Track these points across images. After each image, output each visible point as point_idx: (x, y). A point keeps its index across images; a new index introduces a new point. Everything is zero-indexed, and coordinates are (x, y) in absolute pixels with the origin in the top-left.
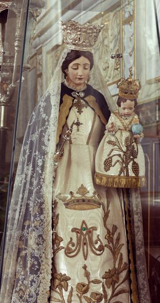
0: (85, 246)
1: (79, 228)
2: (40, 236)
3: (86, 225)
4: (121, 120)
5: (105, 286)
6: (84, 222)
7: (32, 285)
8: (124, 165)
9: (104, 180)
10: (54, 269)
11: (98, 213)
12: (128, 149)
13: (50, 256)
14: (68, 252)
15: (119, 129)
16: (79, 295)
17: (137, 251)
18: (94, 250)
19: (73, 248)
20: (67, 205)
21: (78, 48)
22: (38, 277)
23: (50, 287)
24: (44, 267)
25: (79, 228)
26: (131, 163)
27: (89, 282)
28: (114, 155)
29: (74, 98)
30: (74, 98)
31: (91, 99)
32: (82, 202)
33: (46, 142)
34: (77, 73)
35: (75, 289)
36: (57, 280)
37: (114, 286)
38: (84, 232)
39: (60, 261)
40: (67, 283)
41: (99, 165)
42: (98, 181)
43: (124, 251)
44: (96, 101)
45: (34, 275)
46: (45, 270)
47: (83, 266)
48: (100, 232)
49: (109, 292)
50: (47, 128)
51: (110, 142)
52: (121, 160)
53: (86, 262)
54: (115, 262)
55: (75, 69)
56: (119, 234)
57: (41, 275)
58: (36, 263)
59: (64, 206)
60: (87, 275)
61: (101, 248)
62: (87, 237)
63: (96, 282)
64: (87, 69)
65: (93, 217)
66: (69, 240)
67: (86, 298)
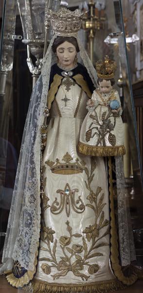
0: (68, 205)
1: (63, 190)
2: (32, 196)
3: (69, 187)
4: (101, 97)
5: (86, 240)
6: (67, 185)
7: (26, 236)
8: (101, 137)
9: (85, 150)
10: (43, 224)
11: (82, 177)
12: (104, 123)
13: (39, 213)
14: (53, 210)
15: (99, 104)
16: (63, 246)
17: (119, 210)
18: (75, 208)
19: (58, 207)
20: (53, 170)
21: (63, 35)
22: (31, 229)
23: (40, 239)
24: (35, 222)
25: (63, 190)
26: (107, 136)
27: (71, 236)
28: (93, 128)
29: (64, 77)
30: (64, 77)
31: (79, 77)
32: (66, 168)
33: (38, 116)
34: (63, 56)
35: (58, 241)
36: (45, 233)
37: (94, 240)
38: (67, 193)
39: (47, 216)
40: (53, 236)
41: (83, 135)
42: (80, 149)
43: (106, 210)
44: (84, 79)
45: (28, 228)
46: (36, 224)
47: (66, 222)
48: (82, 194)
49: (89, 245)
50: (39, 104)
51: (91, 116)
52: (98, 133)
53: (69, 219)
54: (96, 219)
55: (61, 52)
56: (103, 195)
57: (32, 228)
58: (29, 218)
59: (51, 171)
60: (70, 229)
61: (82, 207)
62: (70, 197)
63: (78, 236)
64: (71, 52)
65: (77, 181)
66: (54, 200)
67: (68, 249)
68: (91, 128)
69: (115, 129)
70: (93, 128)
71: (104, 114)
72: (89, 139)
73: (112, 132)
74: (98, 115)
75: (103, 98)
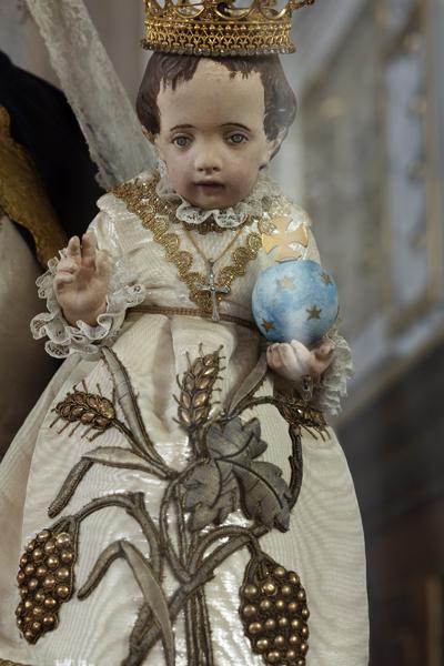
4: (164, 239)
12: (201, 453)
28: (98, 505)
52: (144, 546)
68: (74, 508)
69: (296, 518)
70: (98, 505)
71: (201, 375)
72: (55, 610)
73: (272, 544)
74: (144, 387)
75: (185, 245)
